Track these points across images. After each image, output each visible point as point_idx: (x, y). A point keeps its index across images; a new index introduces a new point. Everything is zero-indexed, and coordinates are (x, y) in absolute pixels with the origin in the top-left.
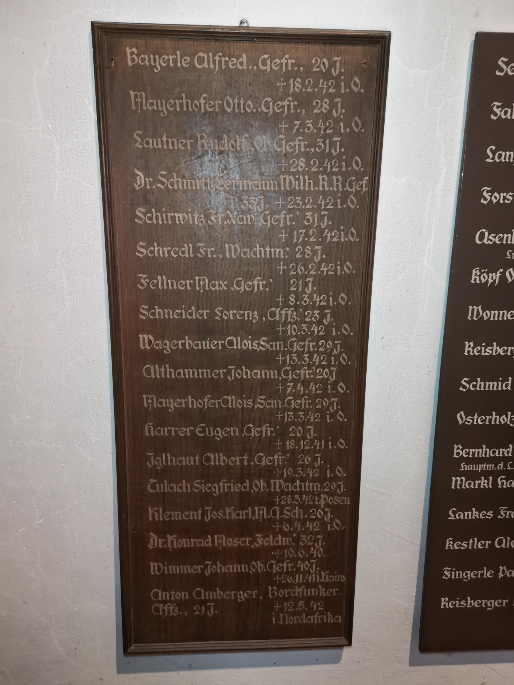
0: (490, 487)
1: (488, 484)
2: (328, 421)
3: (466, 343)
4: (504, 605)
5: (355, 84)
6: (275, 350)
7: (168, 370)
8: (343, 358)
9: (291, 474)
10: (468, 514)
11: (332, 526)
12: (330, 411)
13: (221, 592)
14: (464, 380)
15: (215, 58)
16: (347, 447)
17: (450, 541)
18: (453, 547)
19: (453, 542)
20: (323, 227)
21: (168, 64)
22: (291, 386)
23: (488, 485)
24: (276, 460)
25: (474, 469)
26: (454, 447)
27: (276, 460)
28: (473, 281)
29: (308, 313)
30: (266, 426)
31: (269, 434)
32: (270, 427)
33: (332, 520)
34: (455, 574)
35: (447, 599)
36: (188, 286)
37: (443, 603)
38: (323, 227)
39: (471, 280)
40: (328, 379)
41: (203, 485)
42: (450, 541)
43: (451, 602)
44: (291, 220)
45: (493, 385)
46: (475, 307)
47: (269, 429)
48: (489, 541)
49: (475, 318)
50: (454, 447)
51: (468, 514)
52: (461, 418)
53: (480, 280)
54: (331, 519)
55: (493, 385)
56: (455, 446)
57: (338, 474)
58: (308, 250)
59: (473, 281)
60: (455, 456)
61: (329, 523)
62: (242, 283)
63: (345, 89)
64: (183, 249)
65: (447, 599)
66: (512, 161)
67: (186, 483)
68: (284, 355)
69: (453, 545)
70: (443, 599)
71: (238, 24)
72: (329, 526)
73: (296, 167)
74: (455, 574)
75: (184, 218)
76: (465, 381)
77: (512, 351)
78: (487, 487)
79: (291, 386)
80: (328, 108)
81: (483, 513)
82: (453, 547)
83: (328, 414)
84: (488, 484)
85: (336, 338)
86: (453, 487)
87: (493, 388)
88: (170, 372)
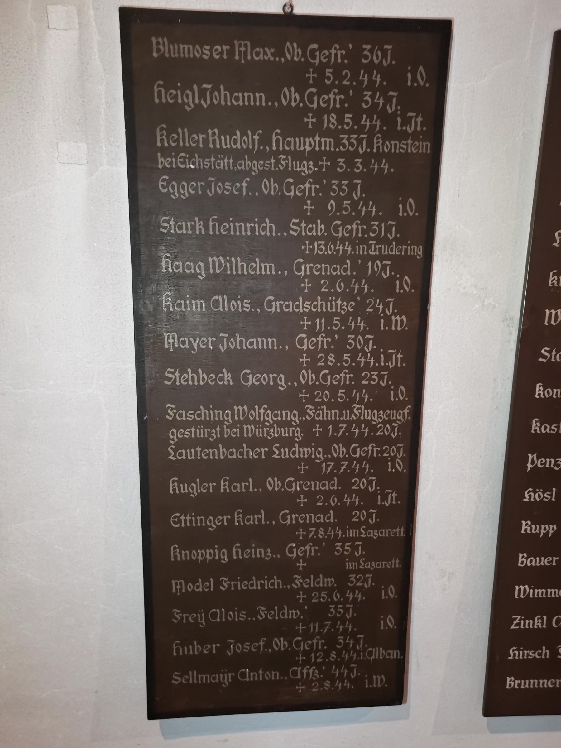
0: (544, 626)
1: (542, 623)
3: (523, 522)
4: (557, 686)
6: (322, 138)
7: (240, 264)
8: (390, 620)
10: (529, 623)
13: (205, 375)
14: (544, 349)
18: (540, 430)
19: (543, 388)
20: (389, 314)
22: (345, 465)
23: (542, 625)
24: (320, 343)
25: (538, 565)
26: (528, 456)
27: (320, 343)
28: (537, 396)
29: (370, 301)
31: (313, 554)
35: (525, 555)
36: (210, 344)
37: (523, 528)
38: (389, 314)
39: (535, 394)
43: (529, 560)
45: (540, 593)
46: (521, 587)
48: (556, 557)
49: (522, 596)
50: (522, 523)
51: (529, 623)
52: (526, 526)
53: (544, 395)
55: (542, 592)
56: (523, 522)
59: (523, 532)
60: (519, 565)
63: (403, 213)
64: (198, 584)
65: (513, 678)
66: (559, 396)
69: (540, 427)
70: (520, 555)
71: (280, 11)
76: (545, 351)
78: (540, 627)
79: (345, 465)
81: (549, 559)
82: (540, 430)
84: (542, 623)
86: (516, 597)
87: (542, 595)
88: (242, 266)
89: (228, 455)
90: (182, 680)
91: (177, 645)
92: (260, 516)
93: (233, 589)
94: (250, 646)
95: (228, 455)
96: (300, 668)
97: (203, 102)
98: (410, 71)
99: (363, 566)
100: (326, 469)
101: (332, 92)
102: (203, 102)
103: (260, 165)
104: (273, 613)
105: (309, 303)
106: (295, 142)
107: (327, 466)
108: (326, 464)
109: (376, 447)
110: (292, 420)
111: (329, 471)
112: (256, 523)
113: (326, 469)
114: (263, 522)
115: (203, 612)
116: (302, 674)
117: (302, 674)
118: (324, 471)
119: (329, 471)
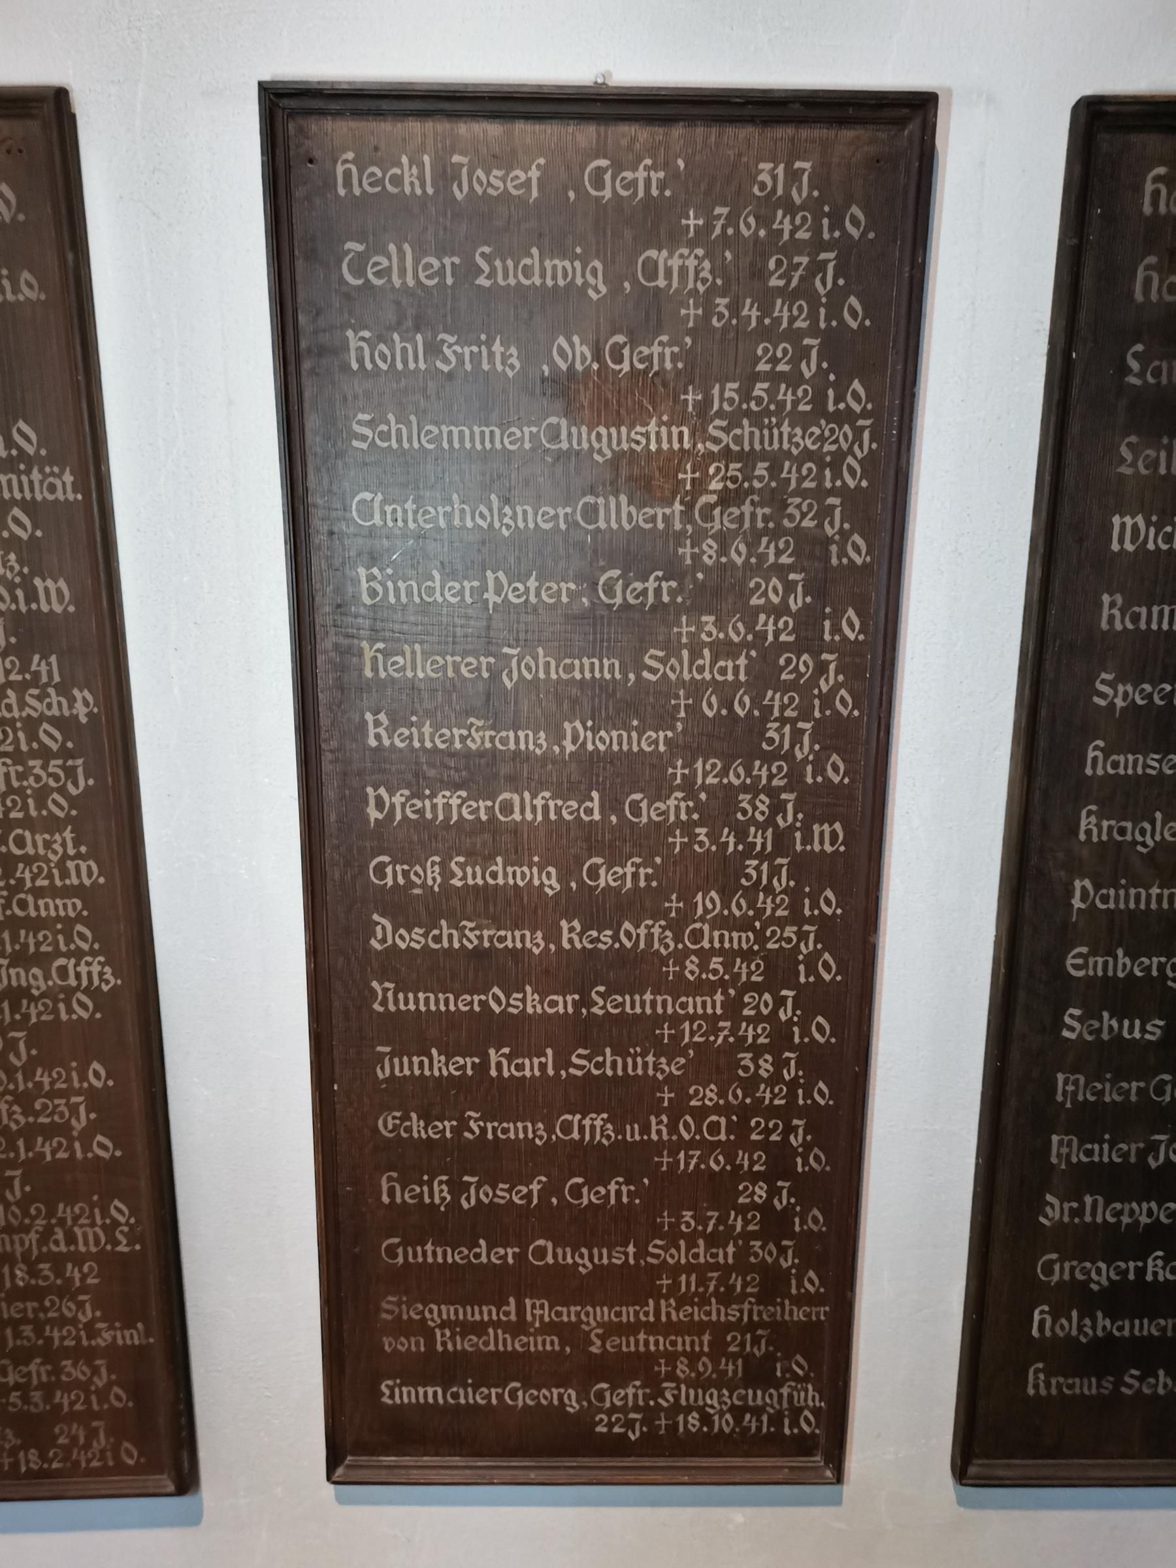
2: (809, 780)
5: (821, 1092)
8: (843, 700)
9: (735, 769)
11: (842, 553)
12: (820, 690)
15: (584, 1122)
16: (839, 978)
17: (1089, 813)
21: (465, 1073)
30: (617, 1183)
32: (627, 1183)
33: (844, 535)
34: (1127, 896)
36: (467, 593)
40: (796, 950)
41: (404, 1307)
42: (1089, 813)
44: (689, 811)
47: (683, 805)
54: (841, 531)
57: (817, 1036)
58: (763, 803)
61: (836, 543)
62: (644, 805)
63: (807, 977)
67: (545, 656)
68: (674, 1153)
72: (834, 548)
73: (703, 1099)
74: (1127, 896)
75: (523, 874)
77: (1171, 896)
80: (771, 1069)
83: (815, 696)
85: (811, 920)
89: (1098, 902)
90: (605, 1003)
91: (390, 1179)
92: (543, 1060)
93: (490, 1136)
94: (509, 1191)
95: (1098, 902)
96: (578, 1116)
97: (756, 1350)
98: (809, 895)
99: (461, 879)
100: (687, 1164)
101: (748, 501)
102: (756, 1350)
103: (375, 269)
104: (385, 262)
105: (506, 1186)
106: (610, 436)
107: (688, 1157)
108: (686, 1154)
109: (14, 765)
110: (578, 1265)
111: (691, 1167)
112: (537, 1073)
113: (687, 1164)
114: (551, 1072)
115: (798, 829)
116: (582, 1129)
117: (582, 1129)
118: (682, 1167)
119: (691, 1167)
